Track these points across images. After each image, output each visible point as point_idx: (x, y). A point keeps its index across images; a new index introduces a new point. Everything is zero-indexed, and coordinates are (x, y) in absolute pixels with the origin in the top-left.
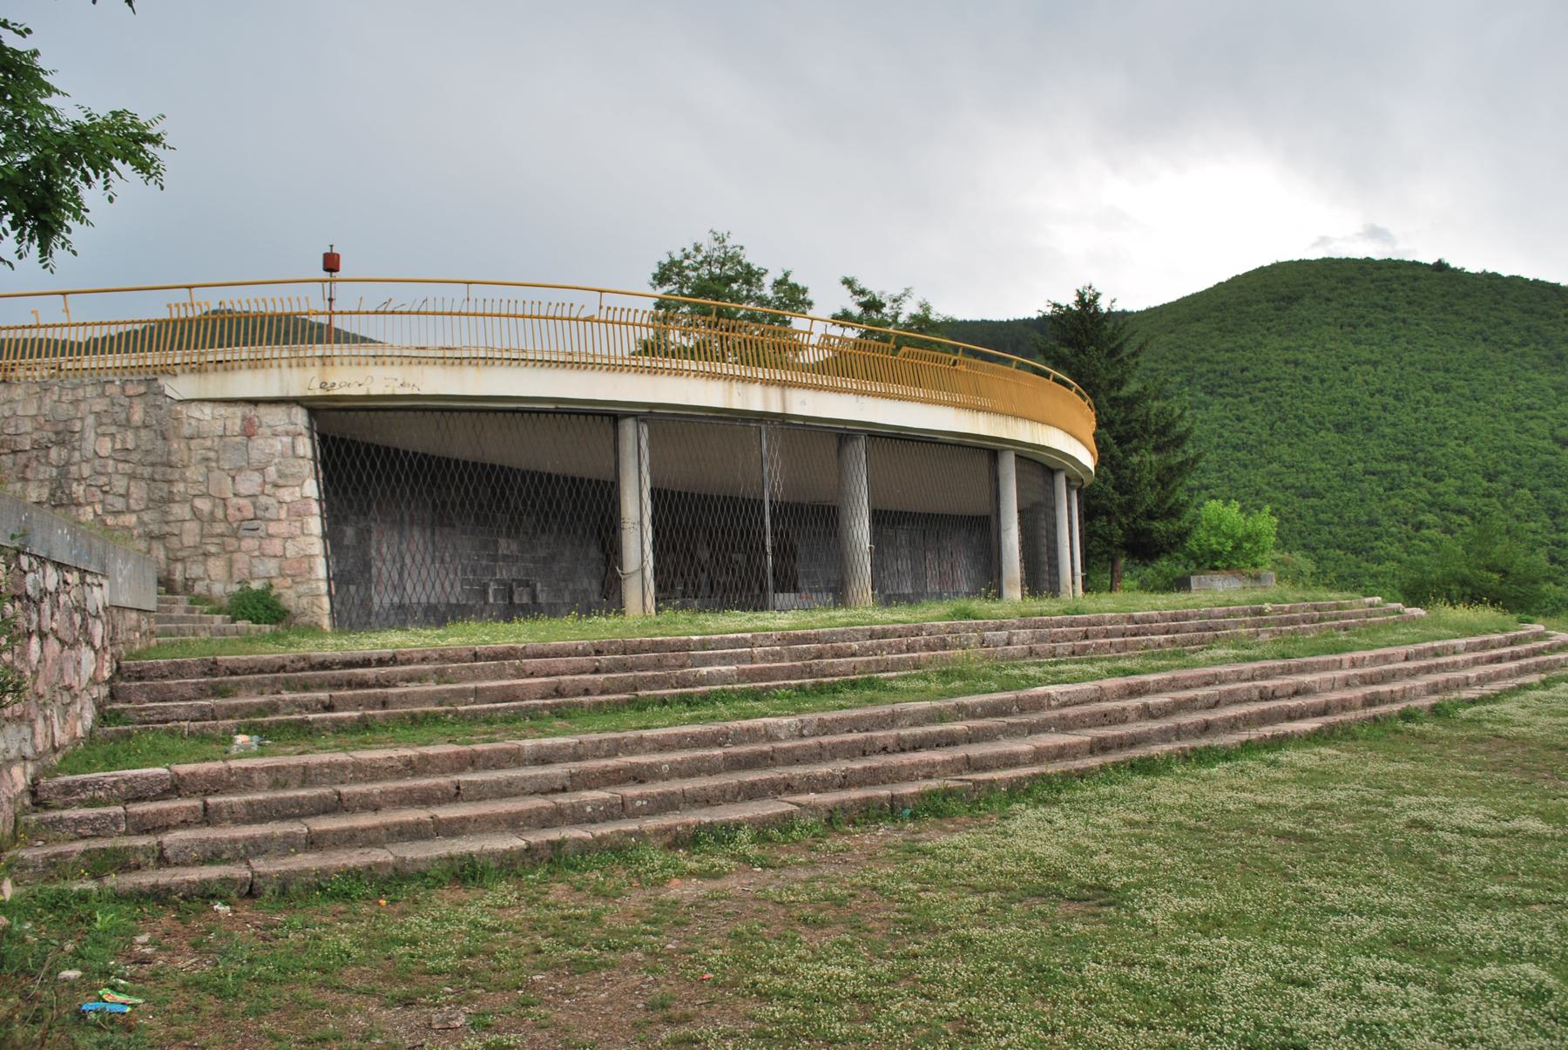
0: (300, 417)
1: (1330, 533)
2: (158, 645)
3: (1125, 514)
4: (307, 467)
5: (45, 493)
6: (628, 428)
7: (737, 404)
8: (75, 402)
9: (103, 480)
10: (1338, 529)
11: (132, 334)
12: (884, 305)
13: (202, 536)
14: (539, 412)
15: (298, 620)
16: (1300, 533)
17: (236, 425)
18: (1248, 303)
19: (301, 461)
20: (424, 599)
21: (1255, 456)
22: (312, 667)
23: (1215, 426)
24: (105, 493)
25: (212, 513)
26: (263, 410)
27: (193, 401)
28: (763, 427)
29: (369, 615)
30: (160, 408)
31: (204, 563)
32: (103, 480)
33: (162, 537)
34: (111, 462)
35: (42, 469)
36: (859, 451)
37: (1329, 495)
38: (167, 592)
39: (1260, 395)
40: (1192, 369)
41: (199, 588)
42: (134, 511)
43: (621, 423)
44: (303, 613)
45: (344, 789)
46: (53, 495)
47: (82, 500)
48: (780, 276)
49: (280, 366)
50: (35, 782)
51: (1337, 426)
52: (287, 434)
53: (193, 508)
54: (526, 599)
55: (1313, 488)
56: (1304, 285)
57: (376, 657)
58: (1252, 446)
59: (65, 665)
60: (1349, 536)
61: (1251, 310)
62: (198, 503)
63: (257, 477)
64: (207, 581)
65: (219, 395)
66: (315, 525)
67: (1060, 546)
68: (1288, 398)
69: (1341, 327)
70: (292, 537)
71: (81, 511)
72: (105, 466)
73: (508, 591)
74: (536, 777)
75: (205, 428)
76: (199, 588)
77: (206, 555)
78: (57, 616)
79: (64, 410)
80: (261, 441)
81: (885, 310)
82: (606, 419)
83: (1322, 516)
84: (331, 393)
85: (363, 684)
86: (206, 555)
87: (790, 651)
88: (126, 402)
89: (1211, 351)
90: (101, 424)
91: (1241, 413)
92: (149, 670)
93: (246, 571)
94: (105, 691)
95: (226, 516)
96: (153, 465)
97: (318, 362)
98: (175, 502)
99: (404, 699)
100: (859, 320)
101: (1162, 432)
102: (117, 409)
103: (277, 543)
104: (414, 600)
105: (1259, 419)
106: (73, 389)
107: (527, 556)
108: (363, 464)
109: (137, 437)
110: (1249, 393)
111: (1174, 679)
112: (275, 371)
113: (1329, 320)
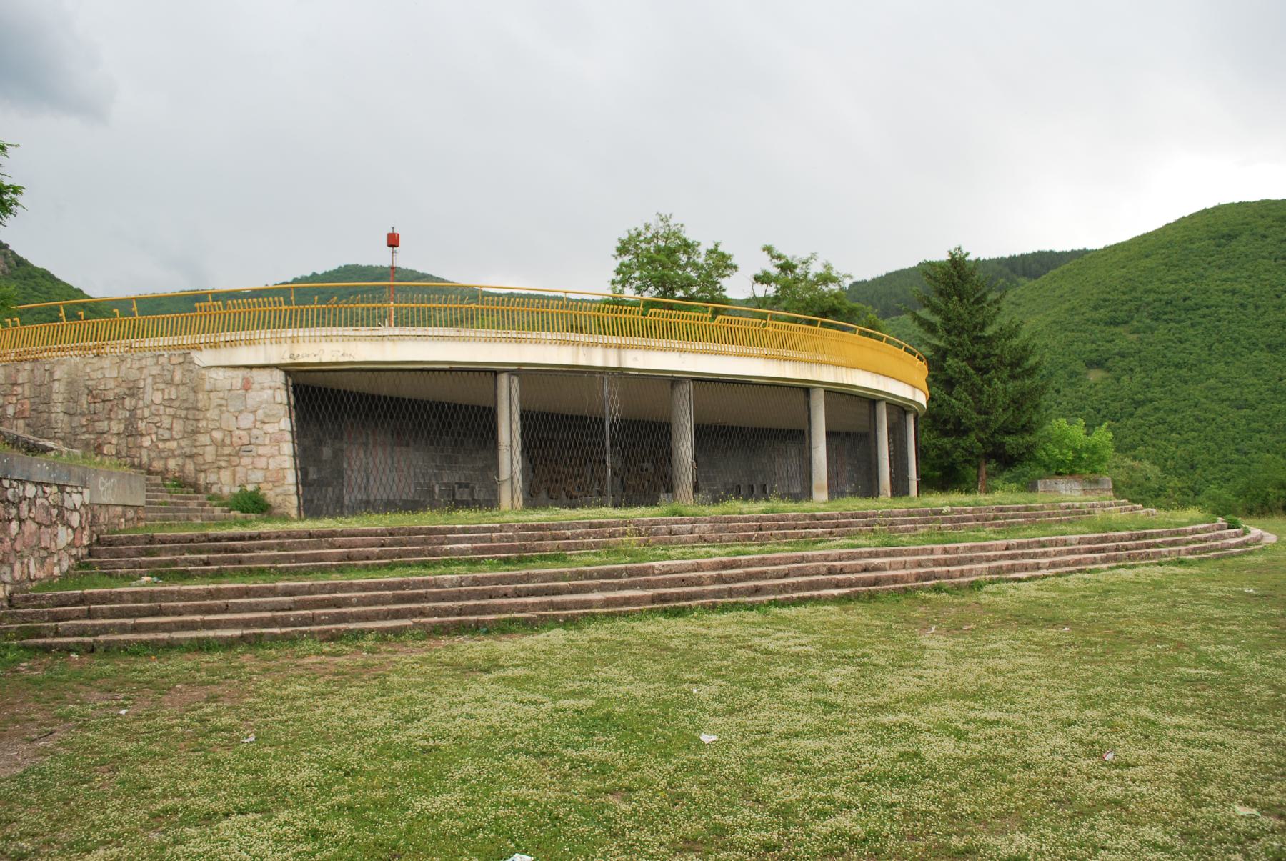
0: (279, 376)
1: (1261, 439)
3: (983, 430)
4: (283, 410)
5: (122, 427)
7: (582, 361)
8: (140, 369)
9: (157, 419)
10: (1268, 436)
12: (795, 267)
13: (217, 455)
15: (276, 511)
16: (1234, 439)
17: (238, 383)
18: (1192, 241)
20: (385, 497)
21: (1194, 373)
22: (210, 541)
23: (1159, 347)
25: (223, 440)
28: (605, 377)
29: (342, 507)
30: (192, 371)
32: (157, 419)
34: (162, 407)
35: (120, 412)
36: (686, 391)
37: (1260, 406)
38: (195, 492)
39: (1201, 320)
40: (1140, 299)
41: (215, 489)
43: (499, 377)
44: (279, 507)
45: (163, 604)
46: (126, 429)
47: (144, 432)
48: (711, 247)
50: (11, 594)
51: (1269, 346)
52: (271, 388)
53: (211, 437)
55: (1246, 400)
56: (1242, 224)
58: (1192, 365)
59: (43, 536)
60: (1277, 442)
61: (1194, 246)
63: (251, 417)
66: (288, 448)
68: (1225, 323)
69: (1275, 260)
70: (272, 456)
71: (144, 439)
72: (158, 410)
73: (450, 491)
75: (219, 384)
76: (215, 489)
77: (220, 468)
78: (33, 510)
79: (133, 374)
81: (798, 271)
82: (488, 374)
83: (1254, 425)
85: (234, 550)
86: (220, 468)
87: (519, 536)
88: (171, 368)
89: (1157, 283)
90: (156, 383)
91: (1184, 336)
94: (85, 552)
96: (187, 409)
97: (289, 341)
100: (776, 280)
102: (166, 372)
105: (1198, 341)
107: (470, 466)
109: (178, 391)
110: (1191, 319)
113: (1264, 254)
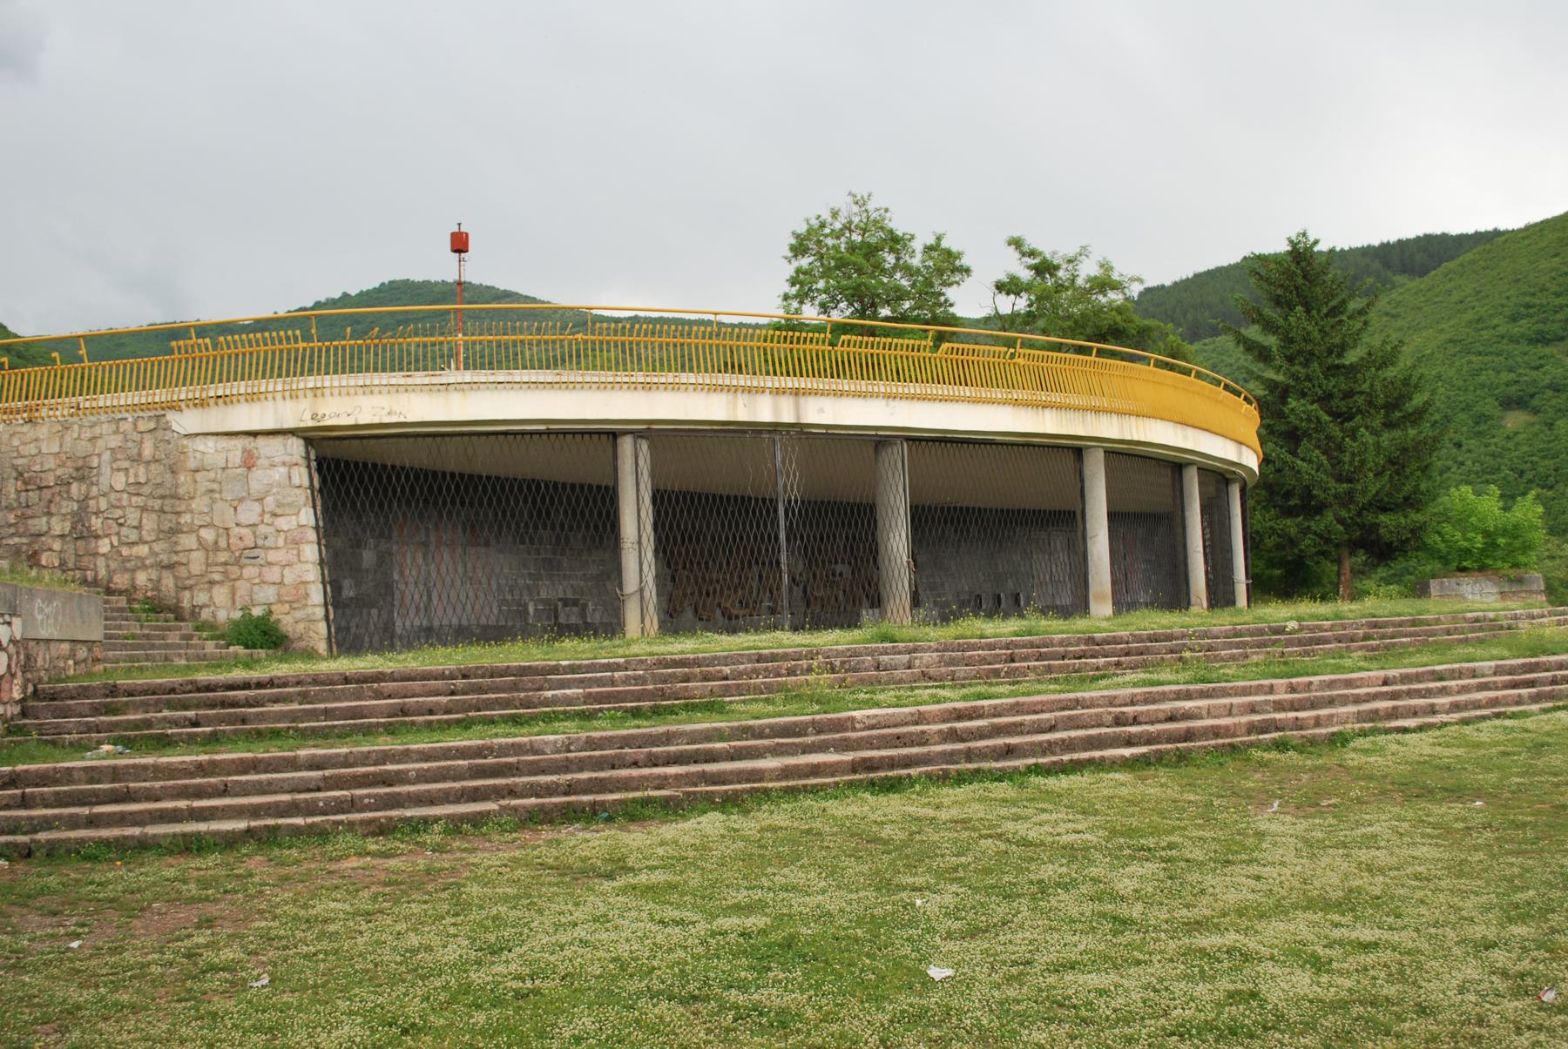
0: (296, 446)
2: (105, 670)
3: (1344, 505)
4: (303, 496)
5: (67, 526)
6: (626, 444)
7: (742, 416)
8: (93, 439)
11: (77, 392)
13: (208, 565)
14: (531, 433)
15: (296, 645)
17: (236, 458)
19: (296, 490)
22: (199, 690)
24: (121, 525)
25: (216, 543)
26: (261, 441)
27: (198, 435)
28: (777, 438)
29: (392, 638)
30: (168, 442)
31: (210, 590)
33: (170, 567)
34: (125, 496)
35: (64, 503)
38: (176, 619)
41: (205, 614)
42: (146, 542)
43: (619, 440)
44: (300, 638)
45: (132, 785)
46: (74, 528)
47: (100, 533)
48: (931, 241)
49: (274, 398)
52: (284, 464)
53: (198, 538)
54: (573, 620)
57: (254, 681)
62: (204, 533)
63: (257, 507)
64: (212, 608)
65: (220, 430)
66: (311, 552)
67: (1190, 550)
70: (288, 565)
71: (100, 542)
72: (119, 500)
74: (293, 778)
75: (209, 460)
76: (205, 614)
77: (212, 583)
79: (83, 448)
80: (260, 472)
81: (1061, 273)
82: (604, 437)
84: (321, 424)
85: (235, 704)
86: (212, 583)
88: (137, 437)
90: (115, 460)
92: (61, 692)
93: (247, 598)
95: (229, 545)
96: (163, 497)
97: (309, 394)
98: (183, 532)
99: (261, 717)
100: (1028, 288)
101: (1391, 406)
102: (130, 444)
103: (276, 569)
104: (474, 622)
106: (91, 427)
108: (358, 493)
111: (1017, 704)
112: (270, 404)
